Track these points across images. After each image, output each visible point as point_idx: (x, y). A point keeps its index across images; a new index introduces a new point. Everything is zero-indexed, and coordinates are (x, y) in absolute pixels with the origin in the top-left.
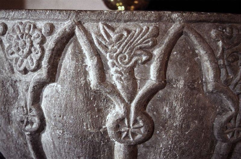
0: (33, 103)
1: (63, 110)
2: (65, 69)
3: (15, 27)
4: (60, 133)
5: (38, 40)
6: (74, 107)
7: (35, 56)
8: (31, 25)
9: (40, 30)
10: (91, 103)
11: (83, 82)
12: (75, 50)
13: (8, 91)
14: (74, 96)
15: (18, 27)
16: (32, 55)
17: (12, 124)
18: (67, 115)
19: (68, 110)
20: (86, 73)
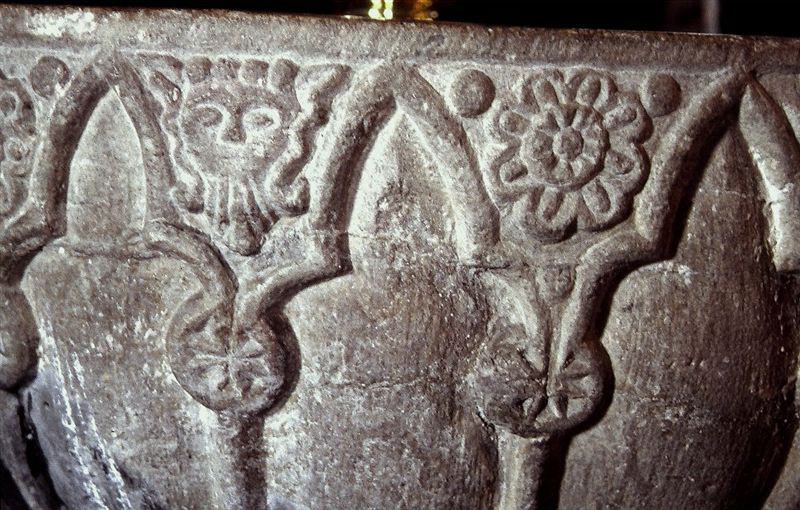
0: (586, 334)
1: (701, 341)
2: (705, 213)
3: (536, 89)
4: (677, 416)
5: (631, 130)
6: (733, 330)
7: (613, 184)
8: (601, 80)
9: (637, 98)
10: (776, 311)
11: (757, 250)
12: (733, 154)
13: (452, 306)
14: (735, 295)
15: (549, 89)
16: (603, 178)
17: (460, 420)
18: (713, 354)
19: (716, 340)
20: (762, 224)
